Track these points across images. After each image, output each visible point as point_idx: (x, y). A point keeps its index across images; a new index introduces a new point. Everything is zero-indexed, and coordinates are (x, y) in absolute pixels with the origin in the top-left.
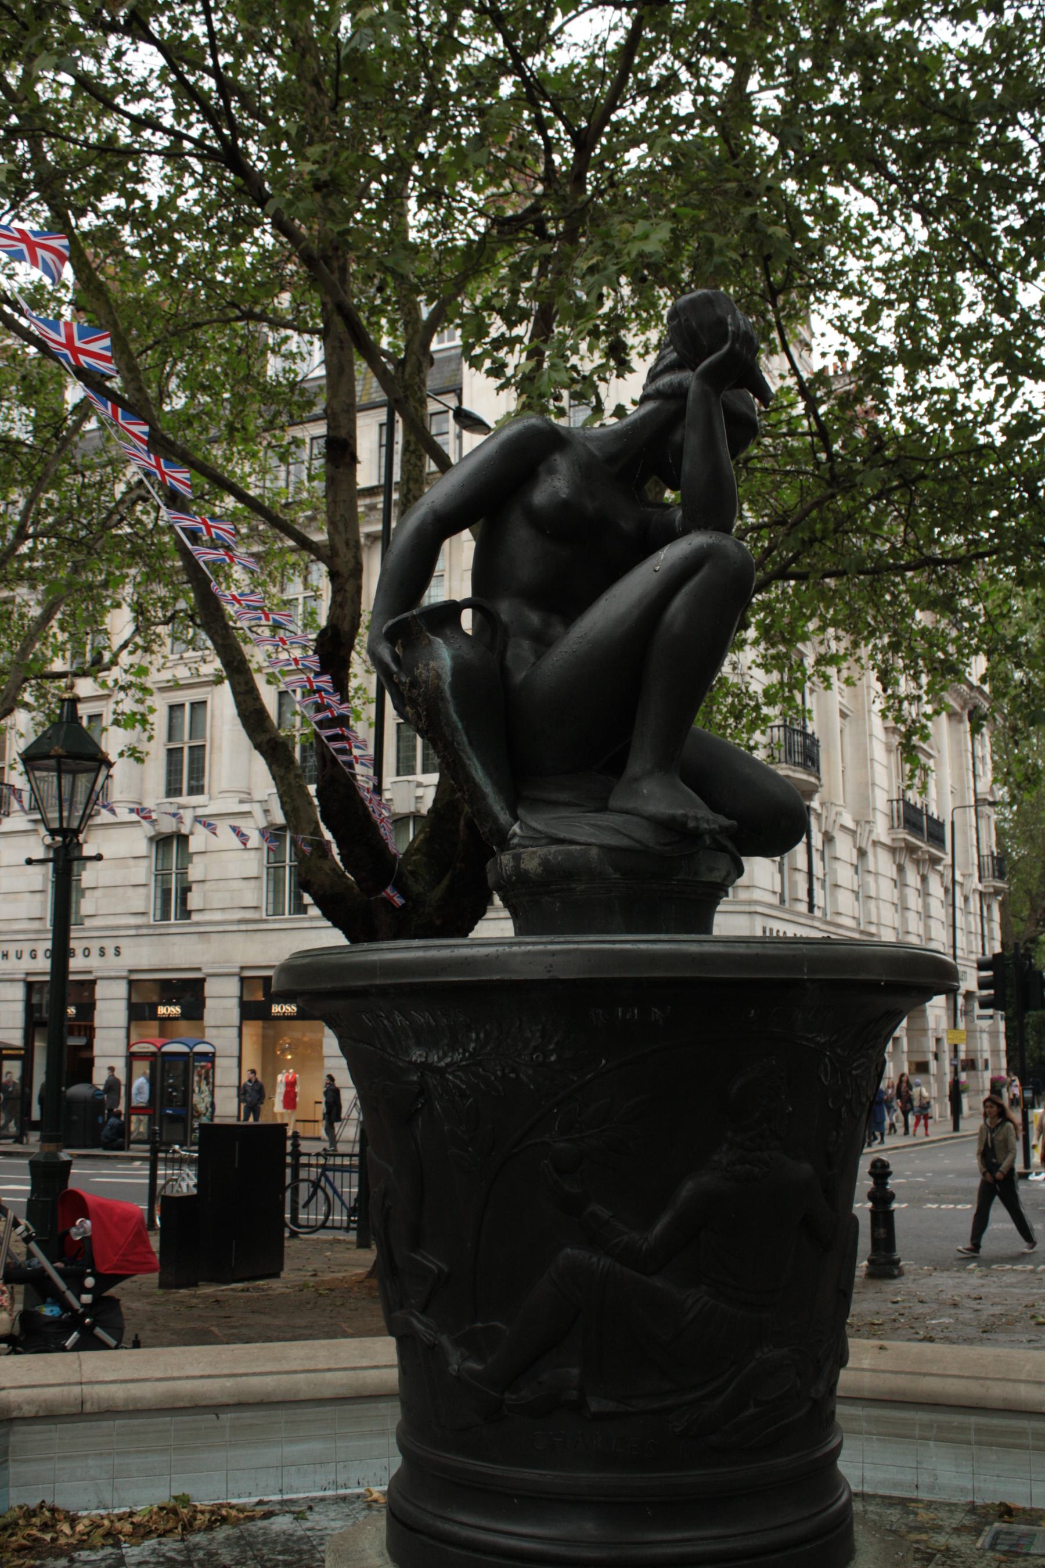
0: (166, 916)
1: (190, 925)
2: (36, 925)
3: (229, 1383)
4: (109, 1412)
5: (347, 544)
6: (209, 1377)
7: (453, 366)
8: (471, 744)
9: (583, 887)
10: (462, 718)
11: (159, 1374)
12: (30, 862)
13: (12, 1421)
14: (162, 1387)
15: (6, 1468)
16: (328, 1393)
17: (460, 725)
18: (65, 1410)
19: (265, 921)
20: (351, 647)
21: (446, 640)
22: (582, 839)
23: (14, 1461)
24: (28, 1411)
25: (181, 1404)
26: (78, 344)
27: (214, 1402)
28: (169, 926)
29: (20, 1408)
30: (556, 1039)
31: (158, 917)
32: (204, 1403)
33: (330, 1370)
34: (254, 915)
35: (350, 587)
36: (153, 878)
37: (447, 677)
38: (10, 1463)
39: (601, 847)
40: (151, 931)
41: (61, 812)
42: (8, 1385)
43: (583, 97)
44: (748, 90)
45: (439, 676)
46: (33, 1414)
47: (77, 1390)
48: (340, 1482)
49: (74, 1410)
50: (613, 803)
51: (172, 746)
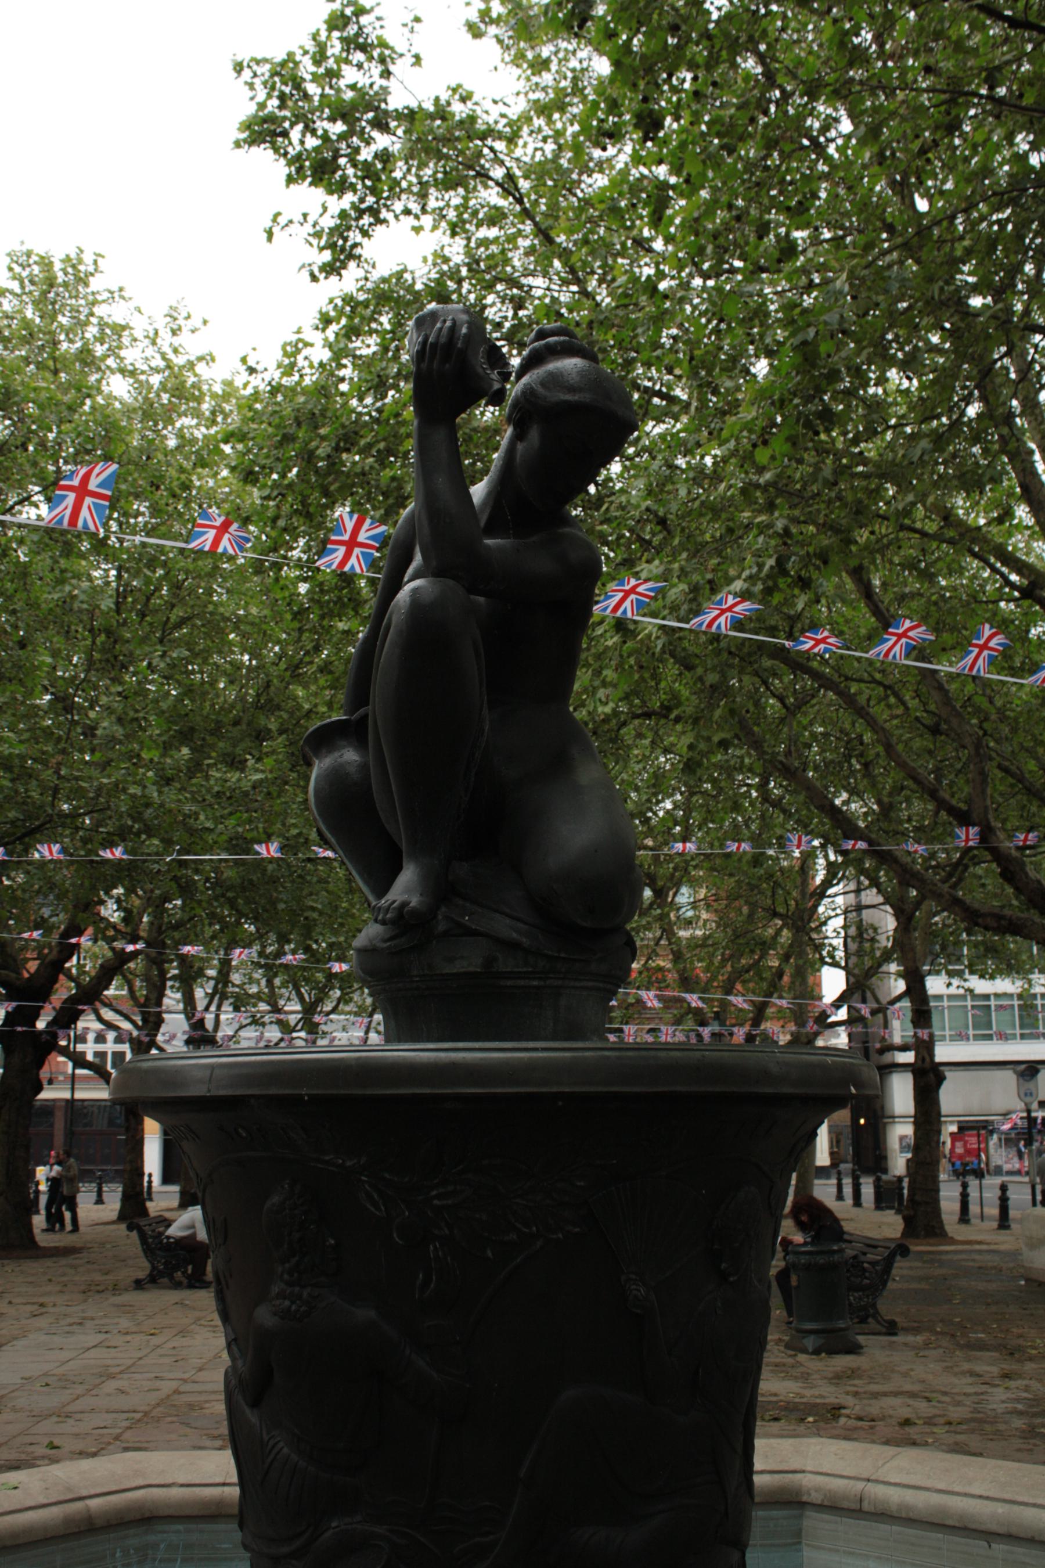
3: (1001, 1509)
4: (883, 1515)
6: (987, 1498)
11: (941, 1486)
12: (378, 4)
13: (803, 1505)
14: (936, 1499)
15: (800, 1550)
18: (845, 1504)
23: (808, 1545)
24: (816, 1498)
25: (950, 1522)
27: (983, 1527)
32: (973, 1526)
38: (805, 1548)
41: (217, 1017)
42: (809, 1468)
44: (37, 962)
47: (860, 1485)
49: (853, 1506)
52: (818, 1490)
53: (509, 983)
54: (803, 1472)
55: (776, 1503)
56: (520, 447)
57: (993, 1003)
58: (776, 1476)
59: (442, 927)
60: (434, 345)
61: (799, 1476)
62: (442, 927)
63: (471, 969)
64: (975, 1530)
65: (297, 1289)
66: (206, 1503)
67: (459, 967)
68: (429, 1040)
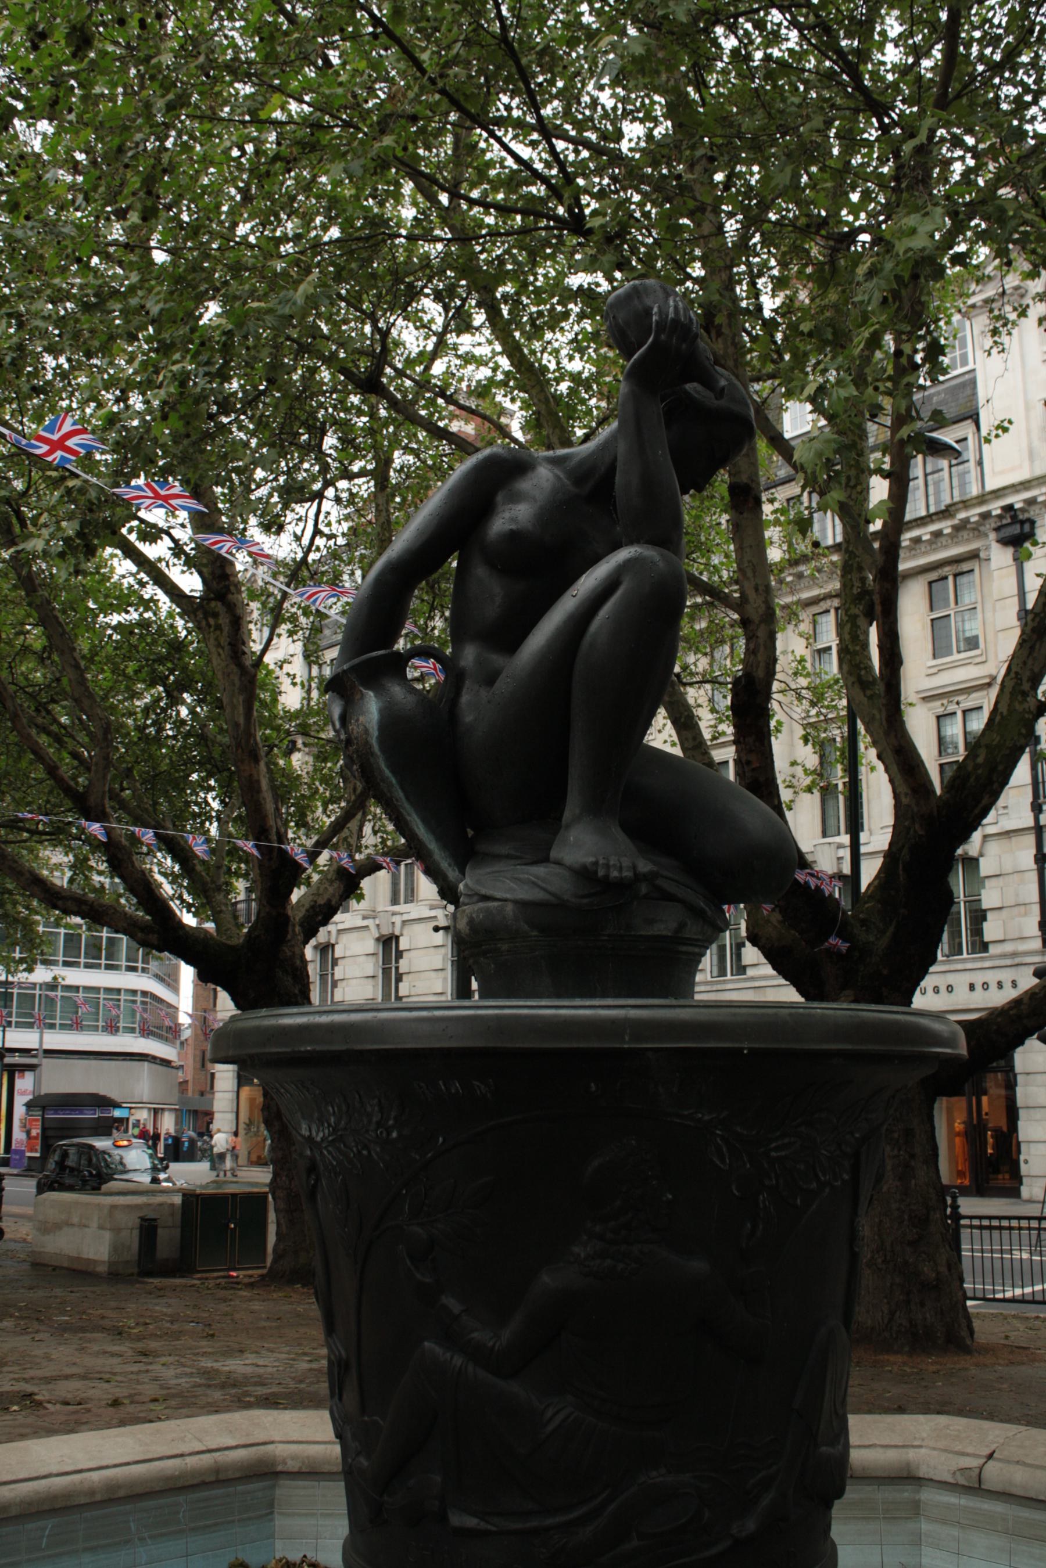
0: (722, 972)
1: (745, 980)
5: (756, 589)
7: (968, 392)
8: (407, 798)
10: (393, 772)
13: (277, 1474)
15: (272, 1520)
17: (394, 781)
18: (326, 1468)
20: (768, 697)
22: (498, 894)
24: (293, 1466)
26: (55, 437)
28: (725, 982)
29: (284, 1463)
30: (393, 1114)
31: (715, 974)
35: (761, 633)
37: (375, 732)
38: (276, 1516)
39: (516, 902)
40: (708, 988)
42: (277, 1439)
45: (366, 731)
46: (296, 1469)
50: (554, 854)
52: (294, 1458)
54: (272, 1442)
55: (171, 1490)
57: (122, 997)
58: (254, 1449)
61: (270, 1447)
63: (664, 933)
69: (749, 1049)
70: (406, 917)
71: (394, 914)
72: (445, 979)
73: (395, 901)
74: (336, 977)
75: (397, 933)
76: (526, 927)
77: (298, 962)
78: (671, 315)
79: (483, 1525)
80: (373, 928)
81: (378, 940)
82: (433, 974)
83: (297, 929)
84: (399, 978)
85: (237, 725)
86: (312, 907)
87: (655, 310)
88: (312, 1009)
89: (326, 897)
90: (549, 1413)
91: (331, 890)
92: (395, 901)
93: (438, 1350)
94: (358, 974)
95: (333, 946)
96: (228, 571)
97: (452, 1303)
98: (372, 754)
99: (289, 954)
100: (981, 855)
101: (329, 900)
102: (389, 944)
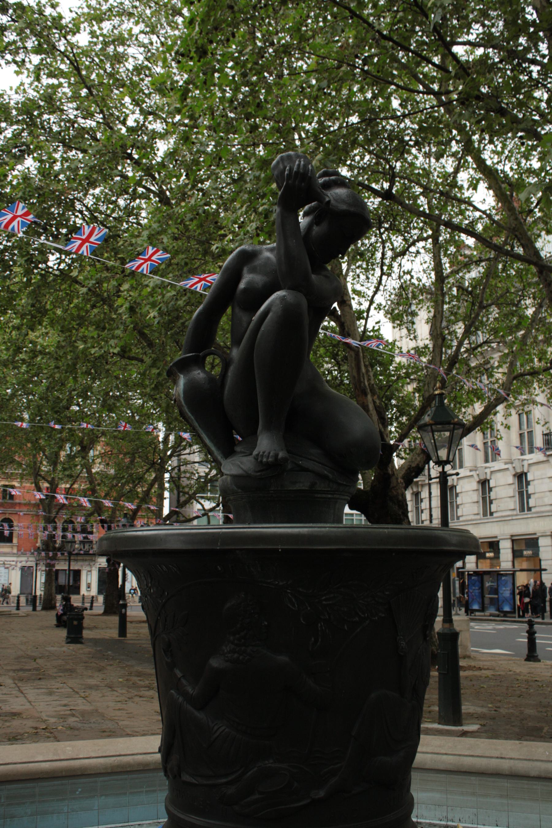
2: (478, 517)
9: (82, 499)
10: (192, 414)
16: (442, 767)
17: (192, 417)
19: (516, 515)
21: (184, 376)
33: (446, 754)
34: (515, 513)
36: (517, 493)
43: (232, 115)
48: (449, 818)
51: (521, 432)
53: (319, 496)
56: (315, 228)
59: (289, 466)
60: (297, 173)
62: (289, 466)
63: (303, 488)
64: (95, 774)
65: (243, 648)
66: (139, 764)
67: (297, 487)
68: (275, 522)
69: (282, 549)
70: (492, 469)
71: (486, 468)
72: (515, 502)
73: (486, 461)
74: (458, 503)
75: (488, 478)
76: (235, 488)
77: (400, 498)
78: (295, 169)
79: (194, 781)
80: (475, 476)
81: (478, 482)
82: (509, 499)
83: (400, 480)
84: (491, 502)
85: (354, 377)
86: (409, 469)
87: (288, 168)
88: (341, 526)
89: (416, 463)
90: (216, 728)
91: (419, 459)
92: (486, 461)
93: (175, 694)
94: (470, 501)
95: (455, 486)
96: (345, 299)
97: (179, 674)
98: (182, 406)
99: (395, 493)
100: (528, 472)
101: (418, 465)
102: (484, 483)
